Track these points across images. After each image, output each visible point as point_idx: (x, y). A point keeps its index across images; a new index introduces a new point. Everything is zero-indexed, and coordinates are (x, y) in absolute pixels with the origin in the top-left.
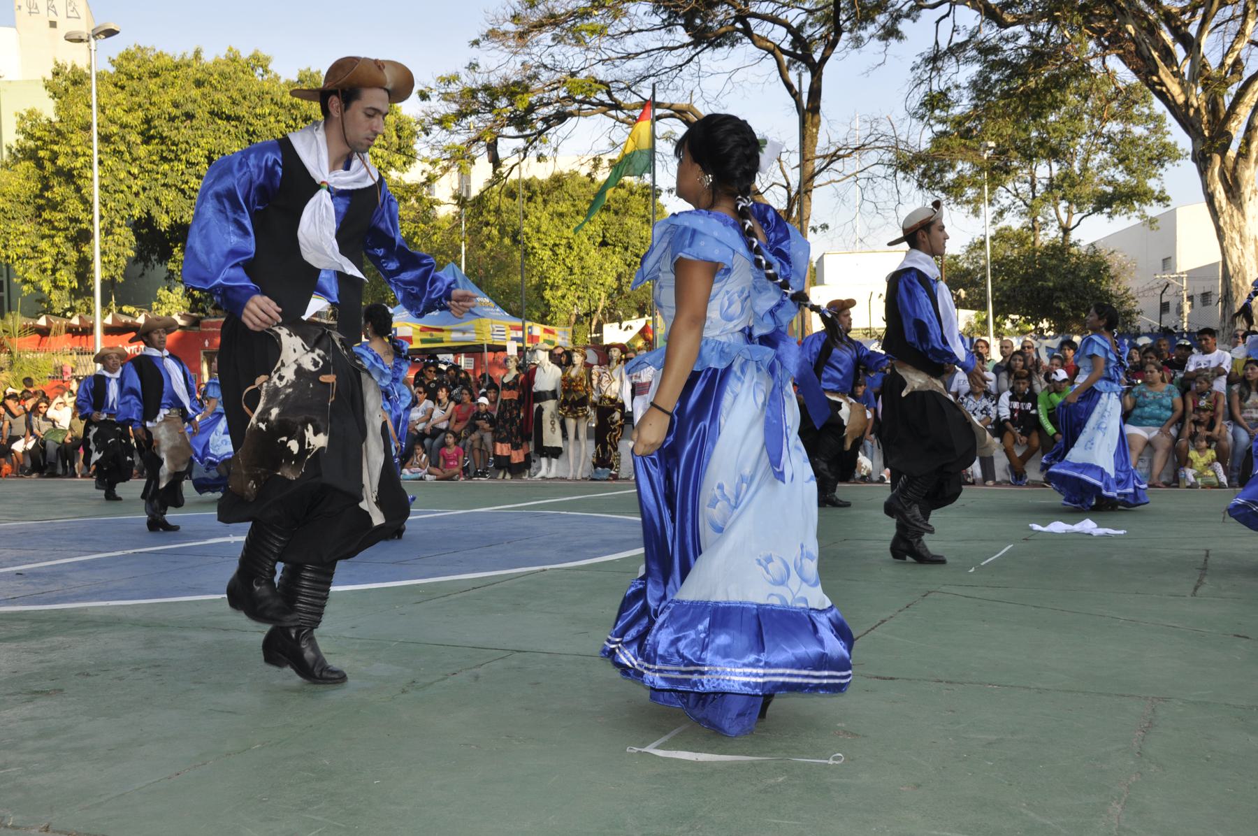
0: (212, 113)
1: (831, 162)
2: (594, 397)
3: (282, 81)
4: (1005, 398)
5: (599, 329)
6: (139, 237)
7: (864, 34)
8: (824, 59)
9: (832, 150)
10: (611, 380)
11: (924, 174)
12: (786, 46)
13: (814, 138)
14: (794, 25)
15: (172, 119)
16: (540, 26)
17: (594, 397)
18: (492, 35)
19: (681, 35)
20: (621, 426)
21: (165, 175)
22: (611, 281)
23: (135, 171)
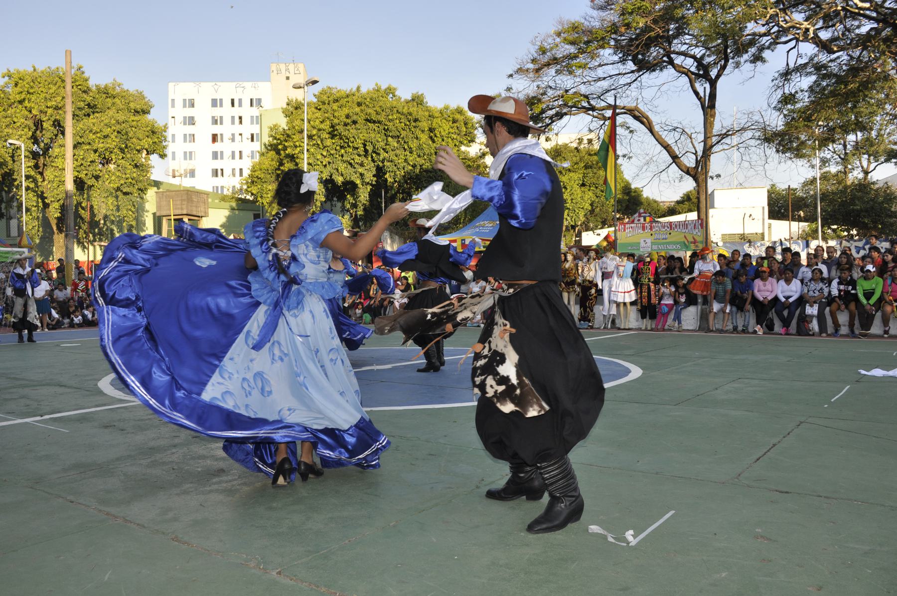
0: (367, 120)
1: (723, 138)
2: (579, 280)
3: (402, 100)
4: (835, 283)
5: (579, 235)
6: (327, 189)
7: (742, 60)
8: (718, 76)
9: (724, 131)
10: (590, 270)
11: (779, 144)
12: (693, 69)
13: (712, 124)
14: (698, 56)
15: (346, 125)
16: (548, 65)
17: (579, 280)
18: (520, 71)
19: (630, 65)
20: (596, 297)
21: (342, 156)
22: (588, 206)
23: (325, 153)
